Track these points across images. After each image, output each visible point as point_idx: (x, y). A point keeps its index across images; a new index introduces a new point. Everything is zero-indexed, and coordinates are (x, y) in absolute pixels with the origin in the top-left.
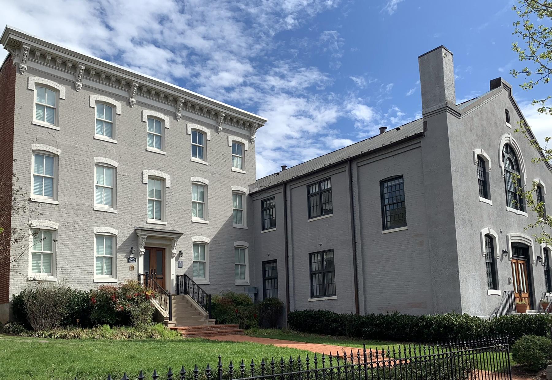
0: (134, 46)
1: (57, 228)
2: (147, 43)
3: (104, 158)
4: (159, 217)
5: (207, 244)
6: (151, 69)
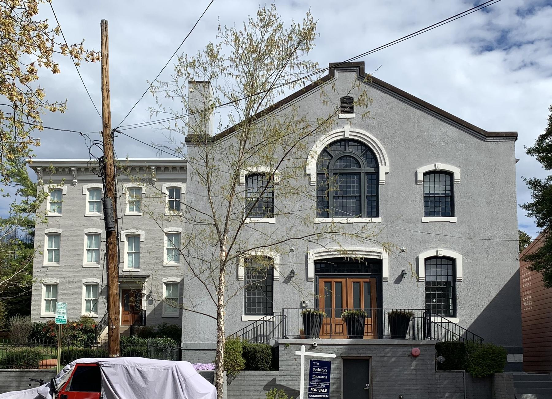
0: (522, 19)
1: (58, 282)
2: (541, 7)
3: (92, 229)
4: (137, 266)
5: (178, 283)
6: (153, 146)
